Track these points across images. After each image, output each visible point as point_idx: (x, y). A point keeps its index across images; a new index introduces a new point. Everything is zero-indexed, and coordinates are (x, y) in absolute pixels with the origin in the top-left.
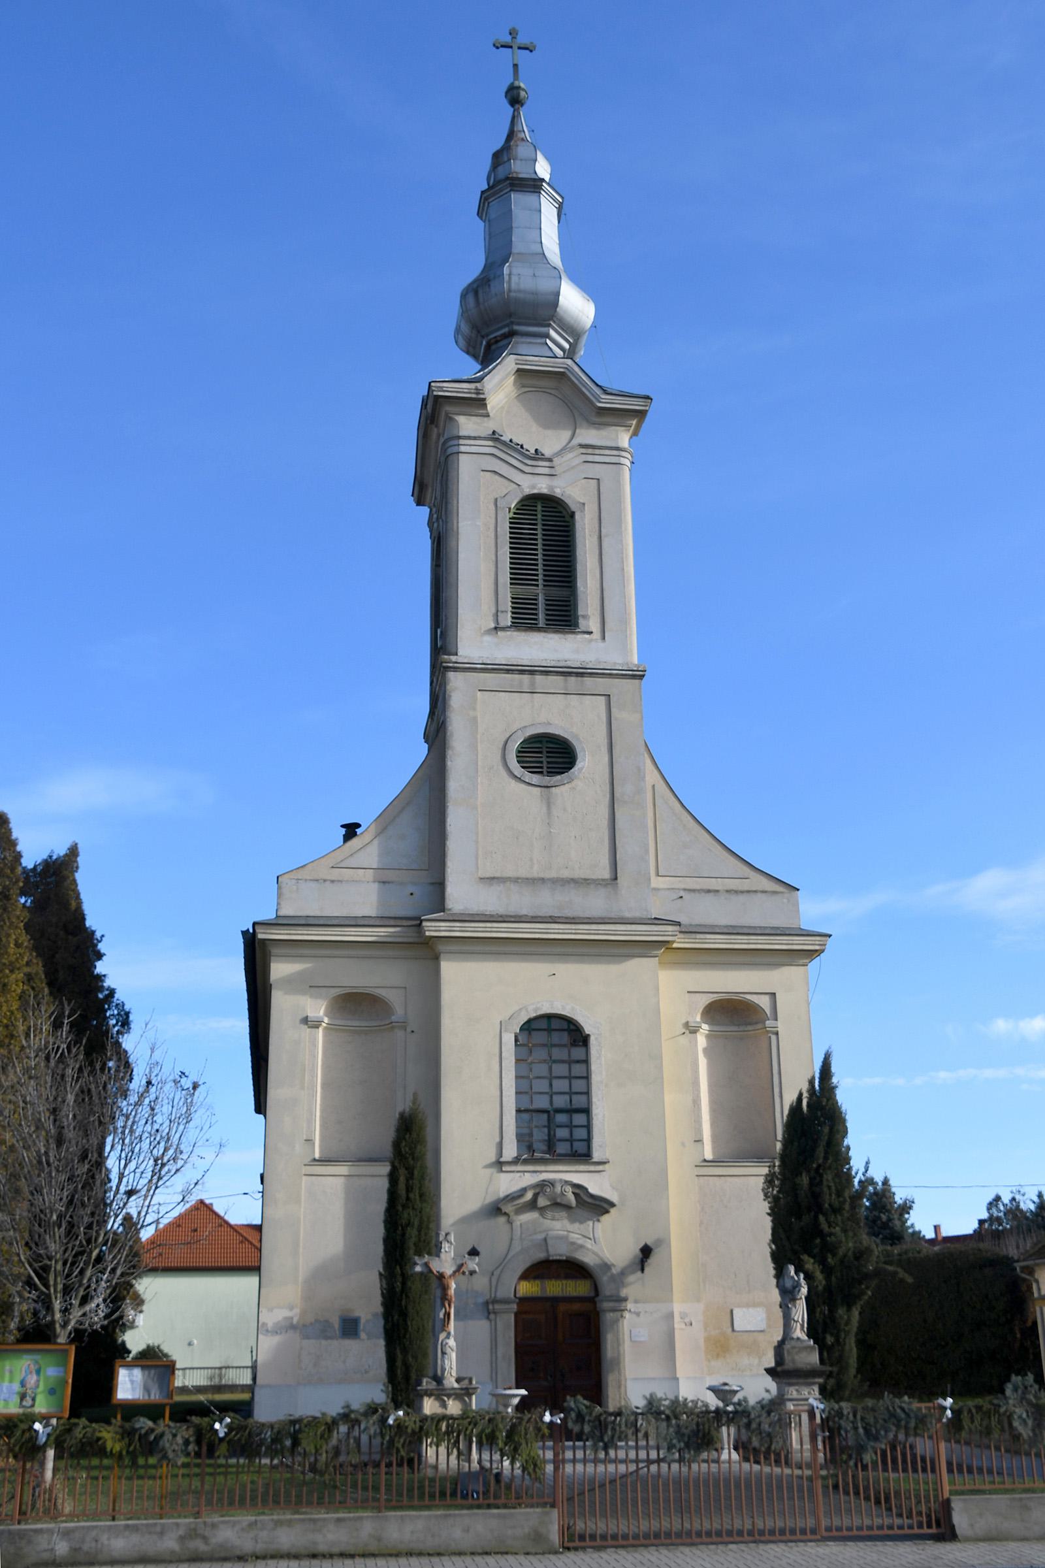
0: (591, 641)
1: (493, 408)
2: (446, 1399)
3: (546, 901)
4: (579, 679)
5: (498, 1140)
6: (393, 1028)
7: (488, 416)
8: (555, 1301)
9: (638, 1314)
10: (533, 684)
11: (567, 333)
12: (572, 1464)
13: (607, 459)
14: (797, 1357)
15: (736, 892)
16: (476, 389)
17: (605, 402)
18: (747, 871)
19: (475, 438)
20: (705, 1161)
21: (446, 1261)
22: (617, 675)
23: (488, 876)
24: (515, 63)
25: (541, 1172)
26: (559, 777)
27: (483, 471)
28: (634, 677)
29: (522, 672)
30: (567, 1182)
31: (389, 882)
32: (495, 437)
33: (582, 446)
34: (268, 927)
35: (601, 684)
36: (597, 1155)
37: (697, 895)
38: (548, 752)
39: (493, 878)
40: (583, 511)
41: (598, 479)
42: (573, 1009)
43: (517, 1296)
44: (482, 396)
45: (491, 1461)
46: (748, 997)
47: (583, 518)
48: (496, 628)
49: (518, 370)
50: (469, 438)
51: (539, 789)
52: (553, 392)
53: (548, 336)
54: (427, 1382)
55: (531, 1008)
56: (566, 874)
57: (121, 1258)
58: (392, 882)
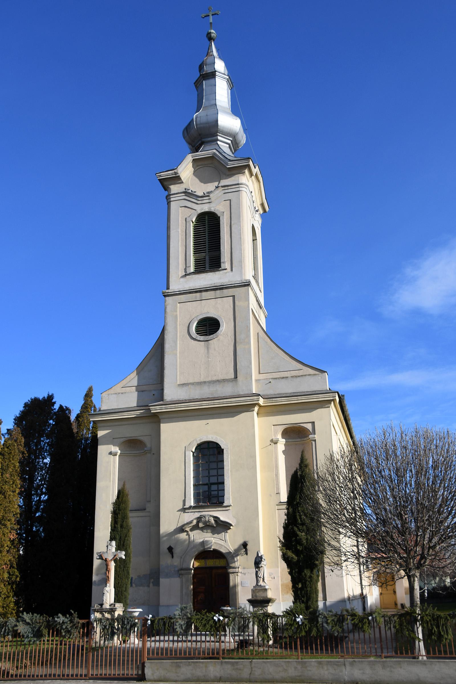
0: (226, 273)
1: (184, 179)
2: (104, 613)
3: (206, 392)
4: (221, 291)
5: (184, 499)
6: (146, 453)
7: (182, 182)
8: (211, 568)
9: (245, 574)
10: (201, 296)
11: (228, 136)
12: (172, 643)
13: (234, 190)
14: (257, 594)
15: (296, 377)
16: (175, 172)
17: (230, 165)
18: (300, 366)
19: (177, 194)
20: (281, 502)
21: (110, 554)
22: (237, 286)
23: (182, 383)
25: (202, 512)
26: (212, 336)
28: (245, 286)
29: (196, 292)
30: (211, 516)
31: (144, 391)
32: (186, 193)
33: (222, 187)
34: (94, 415)
35: (230, 292)
37: (278, 380)
38: (209, 325)
39: (183, 384)
40: (223, 215)
41: (230, 200)
42: (216, 438)
43: (195, 567)
44: (177, 175)
45: (79, 641)
46: (302, 425)
47: (223, 219)
48: (185, 275)
49: (193, 160)
50: (174, 194)
51: (204, 342)
52: (210, 165)
53: (218, 140)
54: (97, 606)
55: (198, 439)
56: (215, 378)
58: (146, 391)
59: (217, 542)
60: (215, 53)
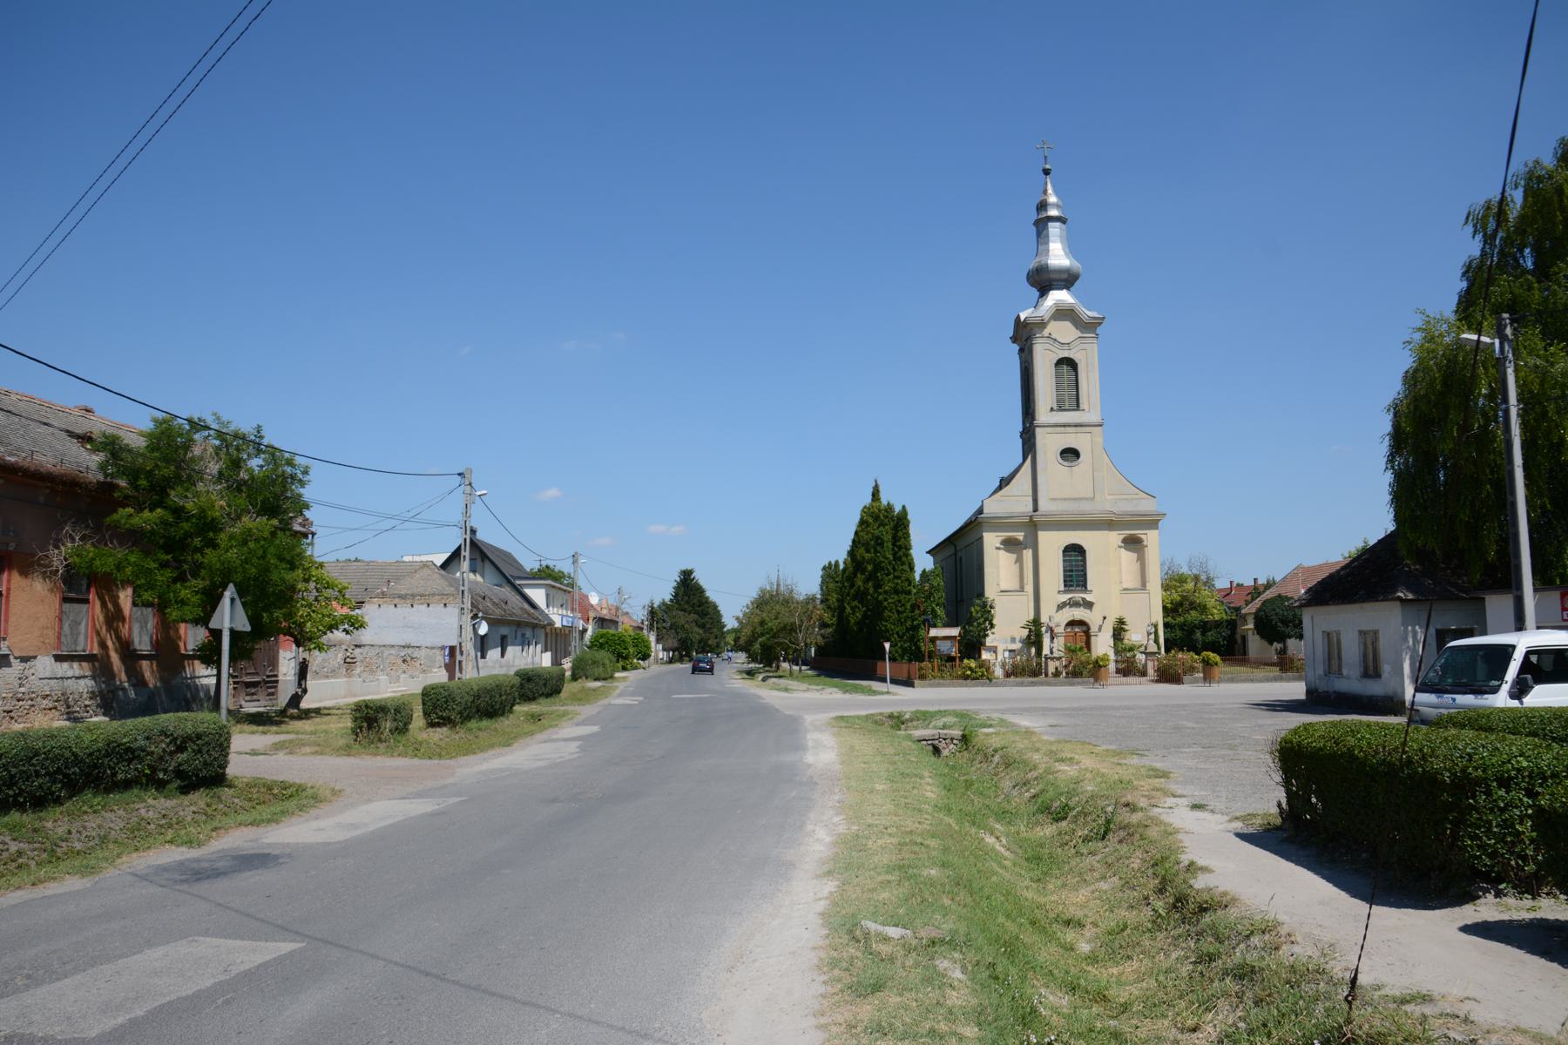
36: (1089, 588)
57: (997, 711)
60: (1050, 191)
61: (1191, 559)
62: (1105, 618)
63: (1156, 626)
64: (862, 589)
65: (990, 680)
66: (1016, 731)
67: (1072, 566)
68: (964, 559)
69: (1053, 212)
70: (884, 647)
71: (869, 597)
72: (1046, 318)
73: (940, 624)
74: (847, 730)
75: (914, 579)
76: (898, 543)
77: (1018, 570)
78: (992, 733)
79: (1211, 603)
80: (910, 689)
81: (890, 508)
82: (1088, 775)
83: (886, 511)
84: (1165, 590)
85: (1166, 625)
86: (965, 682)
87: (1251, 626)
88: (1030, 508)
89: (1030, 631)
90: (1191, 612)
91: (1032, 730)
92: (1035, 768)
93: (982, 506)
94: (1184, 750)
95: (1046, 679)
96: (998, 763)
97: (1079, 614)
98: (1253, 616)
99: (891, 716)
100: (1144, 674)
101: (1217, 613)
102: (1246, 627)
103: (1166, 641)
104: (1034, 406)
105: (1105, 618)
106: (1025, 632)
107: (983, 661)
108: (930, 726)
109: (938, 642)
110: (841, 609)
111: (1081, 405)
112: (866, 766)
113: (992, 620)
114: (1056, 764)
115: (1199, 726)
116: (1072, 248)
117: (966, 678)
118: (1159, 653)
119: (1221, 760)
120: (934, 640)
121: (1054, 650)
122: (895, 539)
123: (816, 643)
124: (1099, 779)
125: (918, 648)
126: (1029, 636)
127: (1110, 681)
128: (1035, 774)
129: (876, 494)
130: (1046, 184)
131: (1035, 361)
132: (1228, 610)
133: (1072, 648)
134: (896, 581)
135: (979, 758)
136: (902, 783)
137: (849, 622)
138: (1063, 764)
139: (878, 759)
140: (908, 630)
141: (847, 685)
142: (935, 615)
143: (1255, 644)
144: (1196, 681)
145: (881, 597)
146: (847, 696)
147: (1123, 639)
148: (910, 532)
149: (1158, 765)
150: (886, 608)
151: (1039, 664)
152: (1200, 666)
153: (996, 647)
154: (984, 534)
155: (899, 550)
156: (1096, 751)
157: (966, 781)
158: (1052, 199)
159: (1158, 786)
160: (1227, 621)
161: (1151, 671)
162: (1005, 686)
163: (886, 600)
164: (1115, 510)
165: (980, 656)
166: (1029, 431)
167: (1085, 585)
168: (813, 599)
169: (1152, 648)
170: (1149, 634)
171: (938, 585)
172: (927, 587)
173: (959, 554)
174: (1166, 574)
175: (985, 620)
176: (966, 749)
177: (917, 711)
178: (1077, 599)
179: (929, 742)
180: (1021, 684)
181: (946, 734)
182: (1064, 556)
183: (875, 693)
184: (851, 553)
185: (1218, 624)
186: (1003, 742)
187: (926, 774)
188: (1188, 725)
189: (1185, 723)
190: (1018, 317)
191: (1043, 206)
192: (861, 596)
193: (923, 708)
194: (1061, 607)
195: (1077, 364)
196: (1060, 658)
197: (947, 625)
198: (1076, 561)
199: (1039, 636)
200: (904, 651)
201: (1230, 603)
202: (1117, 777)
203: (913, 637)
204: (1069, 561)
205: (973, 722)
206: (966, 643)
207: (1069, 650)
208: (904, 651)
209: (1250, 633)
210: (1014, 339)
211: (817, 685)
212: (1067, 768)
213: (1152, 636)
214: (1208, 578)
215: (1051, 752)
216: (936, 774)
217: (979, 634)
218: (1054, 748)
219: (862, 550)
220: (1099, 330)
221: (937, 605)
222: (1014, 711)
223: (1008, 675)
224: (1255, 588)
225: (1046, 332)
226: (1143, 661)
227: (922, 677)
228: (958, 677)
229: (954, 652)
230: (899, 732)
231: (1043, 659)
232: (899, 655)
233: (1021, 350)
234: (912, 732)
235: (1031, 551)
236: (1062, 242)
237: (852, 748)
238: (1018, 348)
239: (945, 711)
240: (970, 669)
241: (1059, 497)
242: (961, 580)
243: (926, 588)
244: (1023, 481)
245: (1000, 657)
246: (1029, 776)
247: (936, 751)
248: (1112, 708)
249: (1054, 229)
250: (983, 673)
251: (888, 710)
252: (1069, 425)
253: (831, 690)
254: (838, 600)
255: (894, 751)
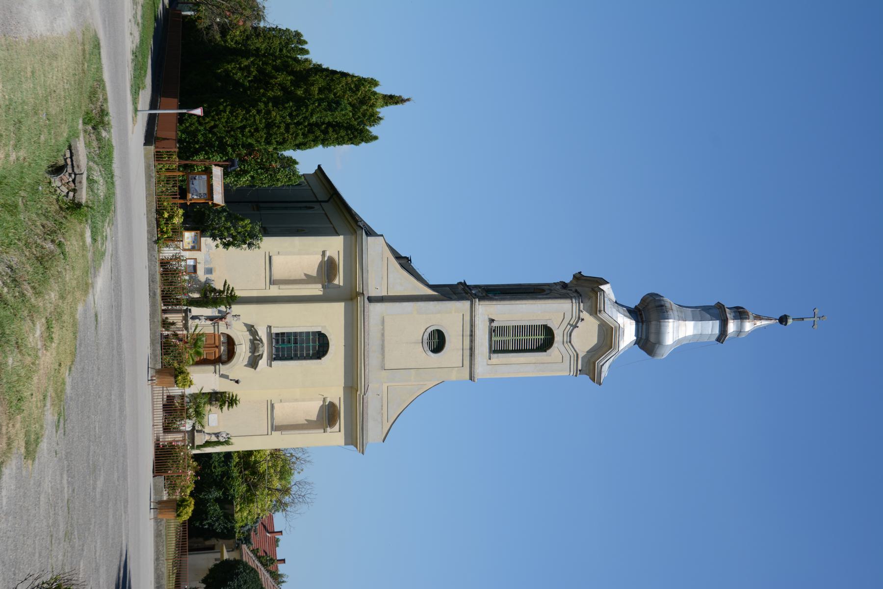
16: (601, 311)
24: (270, 255)
27: (564, 313)
36: (274, 363)
40: (547, 356)
57: (116, 249)
59: (241, 357)
60: (759, 323)
61: (309, 484)
62: (237, 382)
63: (227, 443)
64: (273, 81)
65: (156, 242)
66: (91, 270)
67: (302, 342)
68: (310, 211)
69: (732, 327)
70: (196, 108)
71: (262, 91)
72: (603, 316)
73: (228, 180)
74: (81, 54)
75: (285, 149)
76: (330, 130)
77: (298, 277)
78: (84, 242)
79: (256, 508)
80: (142, 141)
81: (375, 119)
82: (28, 360)
83: (372, 115)
84: (271, 454)
85: (228, 455)
86: (154, 210)
87: (226, 556)
88: (373, 293)
89: (221, 292)
90: (244, 485)
91: (90, 291)
92: (38, 293)
93: (374, 234)
94: (65, 476)
95: (160, 311)
96: (42, 247)
97: (243, 351)
98: (238, 558)
99: (103, 113)
100: (167, 429)
101: (242, 516)
102: (225, 550)
103: (209, 455)
104: (496, 300)
105: (237, 382)
106: (219, 286)
107: (181, 233)
108: (91, 163)
109: (205, 177)
110: (246, 54)
111: (496, 355)
112: (29, 74)
113: (234, 245)
114: (43, 320)
115: (98, 496)
116: (686, 348)
117: (159, 212)
118: (193, 447)
119: (51, 521)
120: (208, 172)
121: (197, 321)
122: (336, 126)
123: (199, 18)
124: (23, 373)
125: (197, 152)
126: (214, 290)
127: (158, 389)
128: (29, 293)
129: (392, 100)
130: (769, 319)
131: (550, 301)
132: (247, 528)
133: (200, 343)
134: (283, 125)
135: (50, 224)
136: (7, 121)
137: (229, 63)
138: (43, 329)
139: (40, 91)
140: (220, 139)
141: (144, 57)
142: (238, 175)
143: (204, 562)
144: (157, 491)
145: (261, 106)
146: (129, 57)
147: (211, 404)
148: (345, 146)
149: (44, 445)
150: (248, 111)
151: (179, 302)
152: (177, 496)
153: (199, 250)
154: (341, 238)
155: (322, 131)
156: (62, 370)
157: (16, 207)
158: (748, 326)
159: (15, 444)
160: (233, 528)
161: (170, 437)
162: (150, 260)
163: (259, 112)
164: (370, 395)
165: (187, 229)
166: (467, 293)
167: (278, 358)
168: (259, 17)
169: (199, 439)
170: (217, 435)
171: (278, 180)
172: (276, 165)
173: (317, 206)
174: (292, 455)
175: (234, 237)
176: (61, 208)
177: (111, 146)
178: (261, 349)
179: (69, 161)
180: (152, 280)
181: (80, 182)
182: (314, 333)
183: (136, 91)
184: (318, 69)
185: (229, 517)
186: (72, 254)
187: (22, 154)
188: (98, 483)
189: (102, 478)
190: (606, 283)
191: (741, 314)
192: (263, 80)
193: (116, 154)
194: (252, 329)
195: (545, 351)
196: (187, 328)
197: (227, 190)
198: (308, 349)
199: (215, 303)
200: (194, 134)
201: (255, 531)
202: (26, 394)
203: (211, 146)
204: (308, 341)
205: (99, 218)
206: (204, 213)
207: (196, 340)
208: (194, 134)
209: (218, 556)
210: (578, 277)
211: (143, 17)
212: (38, 333)
213: (214, 439)
214: (286, 504)
215: (60, 315)
216: (22, 167)
217: (215, 229)
218: (66, 317)
219: (322, 83)
220: (586, 378)
221: (252, 177)
222: (115, 271)
223: (164, 263)
224: (272, 561)
225: (585, 315)
226: (182, 428)
227: (158, 156)
228: (159, 201)
229: (192, 197)
230: (81, 121)
231: (185, 308)
232: (187, 127)
233: (564, 285)
234: (81, 138)
235: (321, 293)
236: (694, 335)
237: (55, 57)
238: (567, 281)
239: (113, 183)
240: (171, 217)
241: (386, 328)
242: (286, 208)
243: (273, 164)
244: (407, 285)
245: (187, 254)
246: (26, 286)
247: (57, 170)
248: (121, 396)
249: (712, 327)
250: (166, 233)
251: (111, 108)
252: (472, 341)
253: (137, 35)
254: (258, 49)
255: (54, 113)
